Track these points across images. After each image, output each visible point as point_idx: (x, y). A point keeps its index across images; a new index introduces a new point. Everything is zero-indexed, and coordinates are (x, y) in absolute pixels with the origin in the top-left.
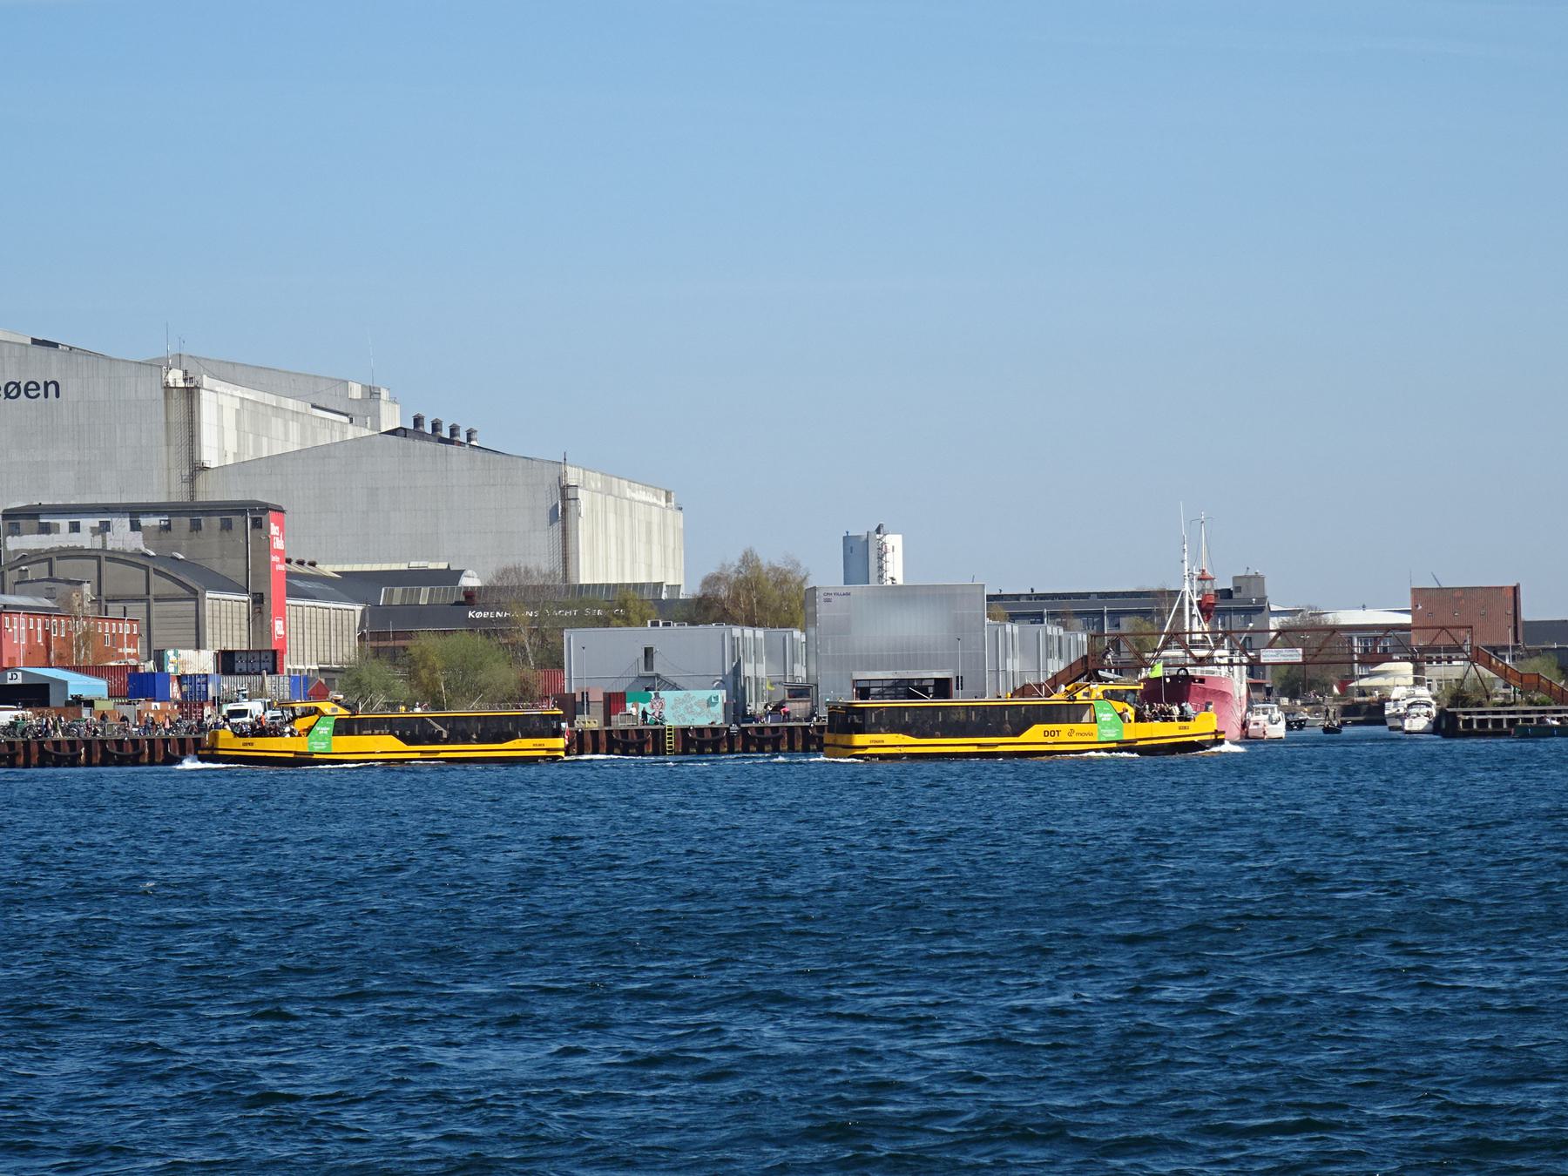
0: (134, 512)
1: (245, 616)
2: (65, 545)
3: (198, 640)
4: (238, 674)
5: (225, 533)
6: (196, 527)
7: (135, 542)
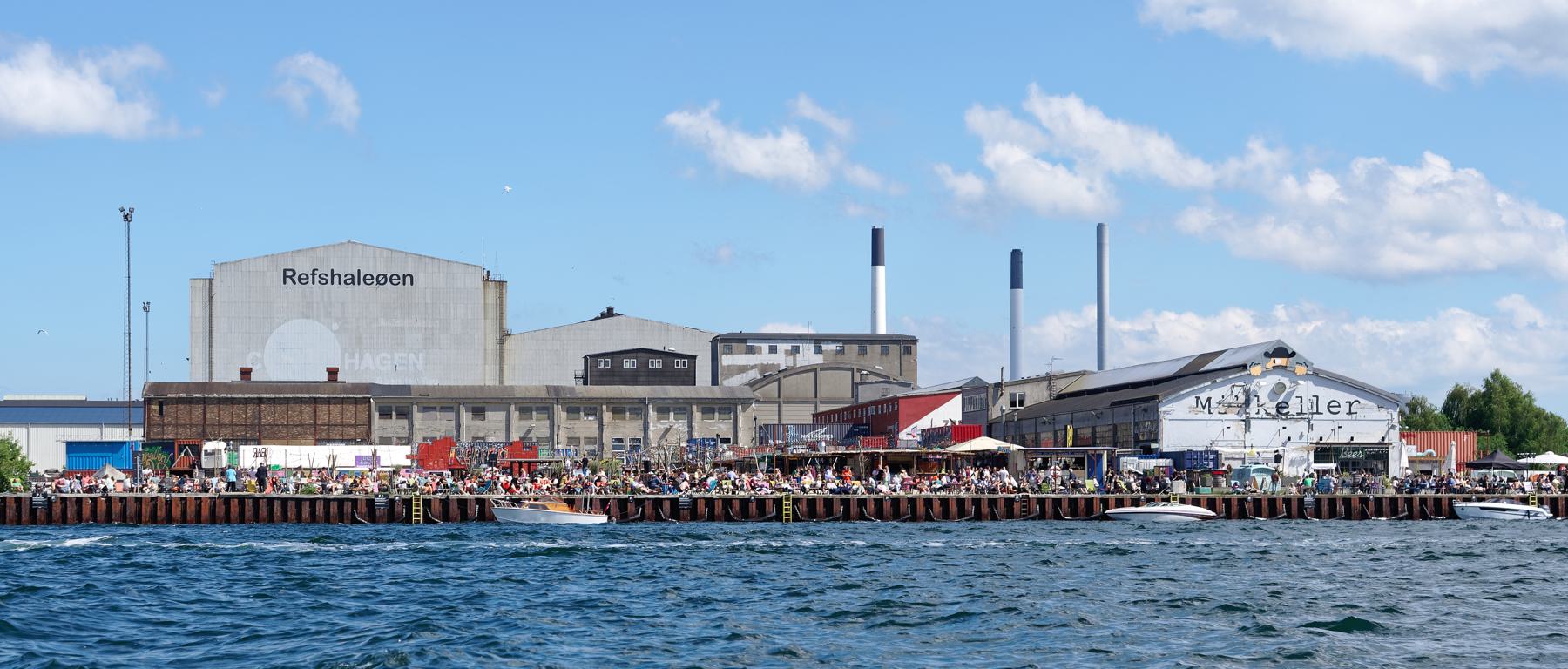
0: (818, 341)
5: (884, 357)
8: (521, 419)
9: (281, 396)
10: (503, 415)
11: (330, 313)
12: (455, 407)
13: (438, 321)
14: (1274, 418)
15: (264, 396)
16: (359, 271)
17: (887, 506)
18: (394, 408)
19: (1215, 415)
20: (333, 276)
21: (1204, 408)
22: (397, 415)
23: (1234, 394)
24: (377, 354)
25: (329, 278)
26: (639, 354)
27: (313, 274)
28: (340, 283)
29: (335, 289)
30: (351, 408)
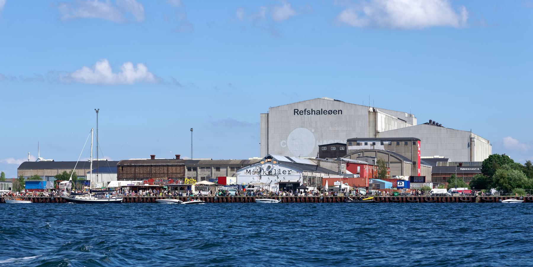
1: (411, 168)
2: (363, 149)
3: (402, 174)
4: (415, 182)
6: (398, 144)
7: (382, 148)
8: (231, 171)
9: (158, 164)
10: (226, 169)
11: (311, 125)
12: (211, 167)
13: (351, 128)
14: (268, 175)
15: (152, 164)
16: (322, 109)
17: (449, 199)
18: (192, 168)
19: (252, 175)
20: (312, 111)
21: (248, 173)
22: (193, 170)
23: (257, 169)
24: (329, 140)
25: (311, 112)
26: (336, 145)
27: (305, 111)
28: (315, 114)
29: (313, 116)
30: (179, 168)
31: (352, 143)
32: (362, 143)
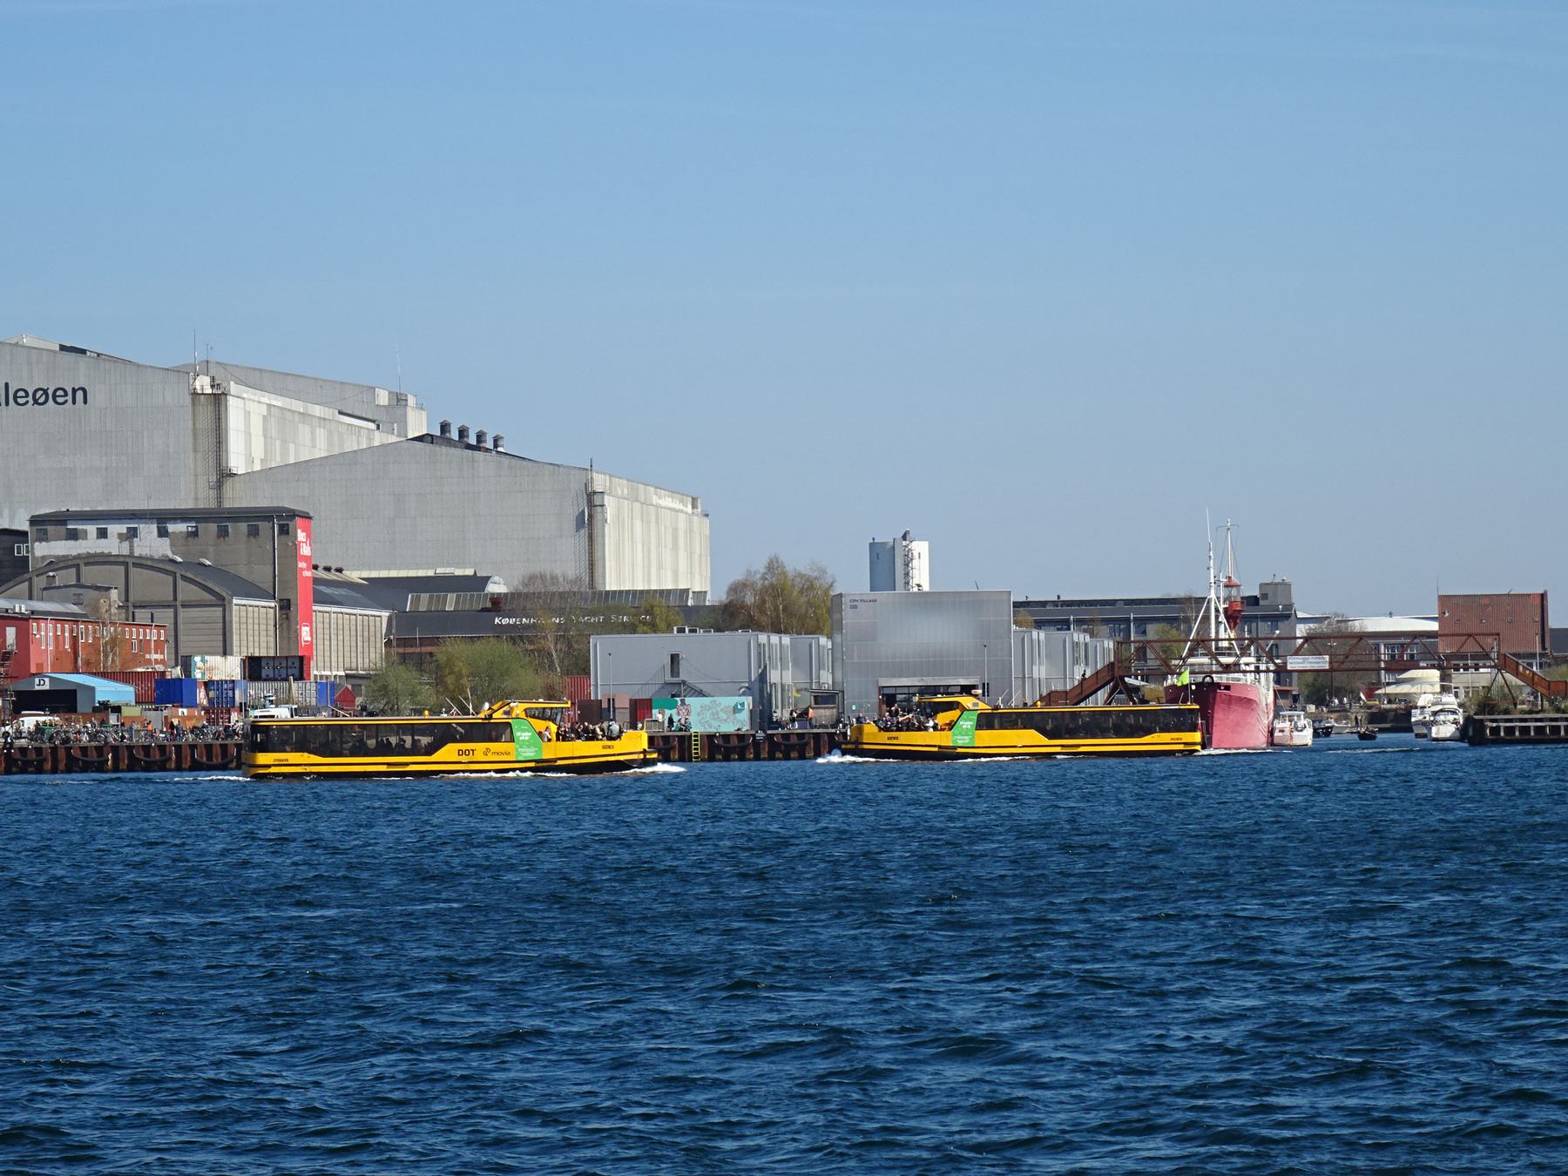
2: (92, 552)
4: (265, 680)
5: (252, 538)
31: (50, 528)
32: (86, 531)
